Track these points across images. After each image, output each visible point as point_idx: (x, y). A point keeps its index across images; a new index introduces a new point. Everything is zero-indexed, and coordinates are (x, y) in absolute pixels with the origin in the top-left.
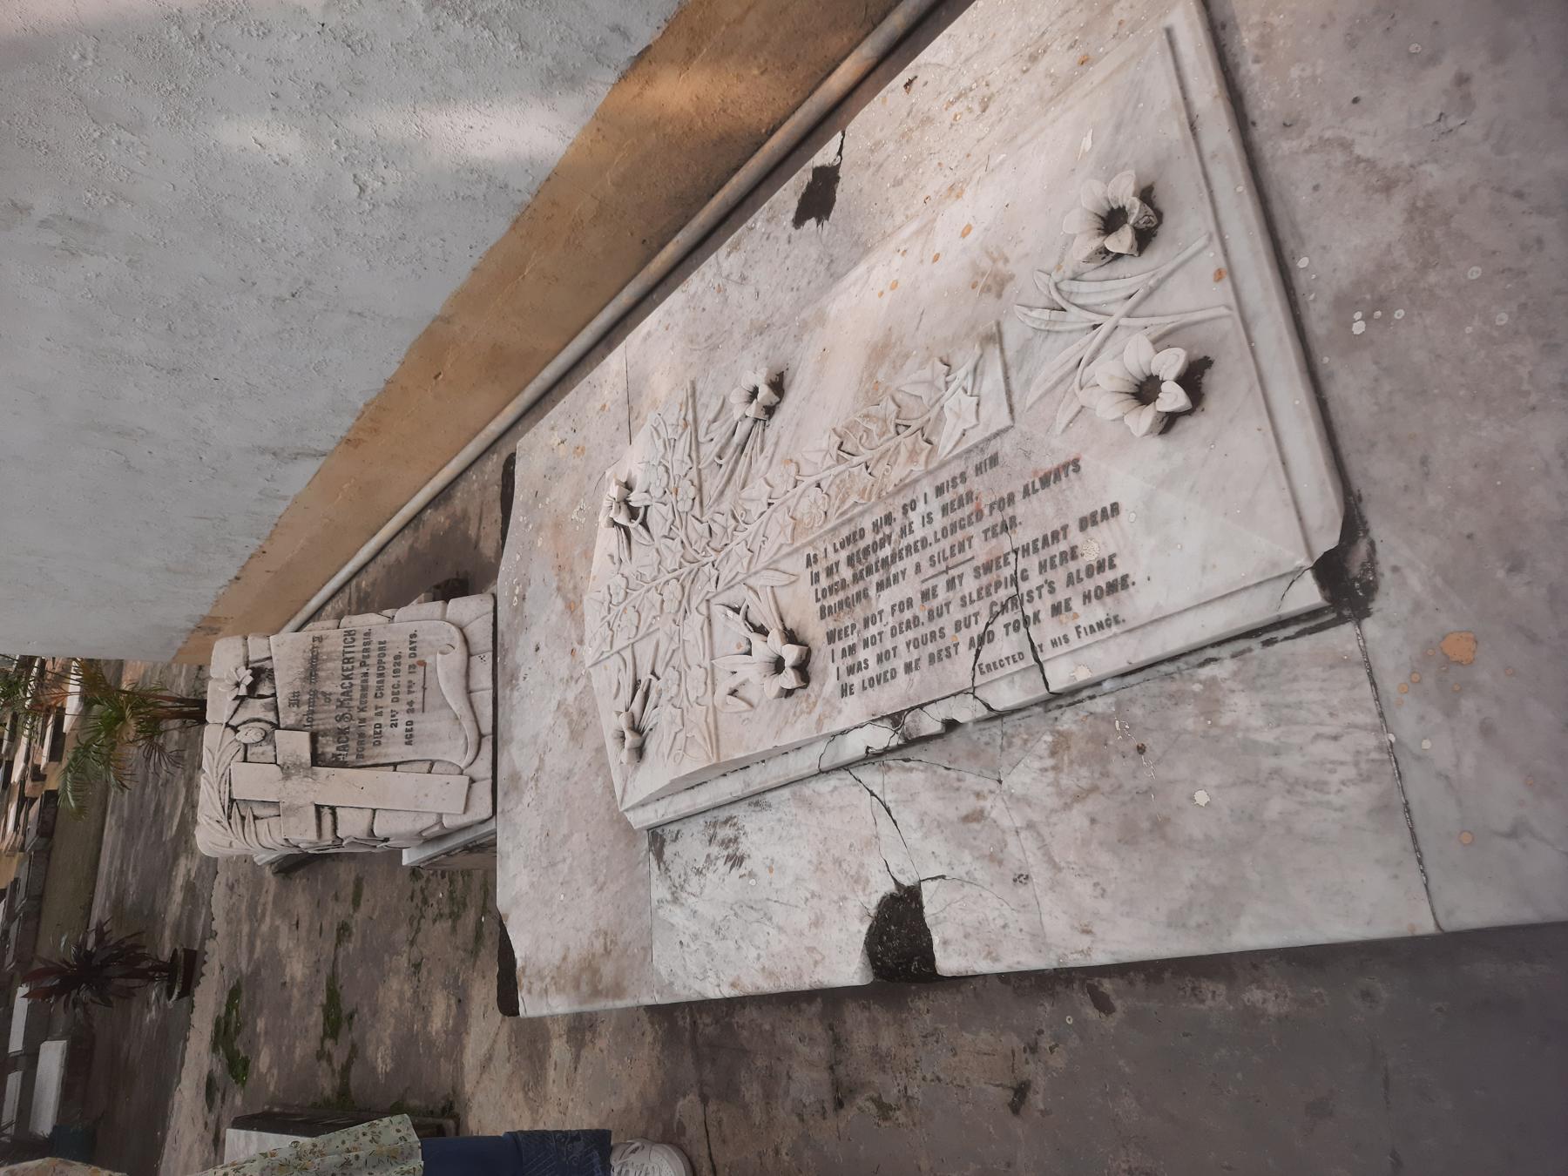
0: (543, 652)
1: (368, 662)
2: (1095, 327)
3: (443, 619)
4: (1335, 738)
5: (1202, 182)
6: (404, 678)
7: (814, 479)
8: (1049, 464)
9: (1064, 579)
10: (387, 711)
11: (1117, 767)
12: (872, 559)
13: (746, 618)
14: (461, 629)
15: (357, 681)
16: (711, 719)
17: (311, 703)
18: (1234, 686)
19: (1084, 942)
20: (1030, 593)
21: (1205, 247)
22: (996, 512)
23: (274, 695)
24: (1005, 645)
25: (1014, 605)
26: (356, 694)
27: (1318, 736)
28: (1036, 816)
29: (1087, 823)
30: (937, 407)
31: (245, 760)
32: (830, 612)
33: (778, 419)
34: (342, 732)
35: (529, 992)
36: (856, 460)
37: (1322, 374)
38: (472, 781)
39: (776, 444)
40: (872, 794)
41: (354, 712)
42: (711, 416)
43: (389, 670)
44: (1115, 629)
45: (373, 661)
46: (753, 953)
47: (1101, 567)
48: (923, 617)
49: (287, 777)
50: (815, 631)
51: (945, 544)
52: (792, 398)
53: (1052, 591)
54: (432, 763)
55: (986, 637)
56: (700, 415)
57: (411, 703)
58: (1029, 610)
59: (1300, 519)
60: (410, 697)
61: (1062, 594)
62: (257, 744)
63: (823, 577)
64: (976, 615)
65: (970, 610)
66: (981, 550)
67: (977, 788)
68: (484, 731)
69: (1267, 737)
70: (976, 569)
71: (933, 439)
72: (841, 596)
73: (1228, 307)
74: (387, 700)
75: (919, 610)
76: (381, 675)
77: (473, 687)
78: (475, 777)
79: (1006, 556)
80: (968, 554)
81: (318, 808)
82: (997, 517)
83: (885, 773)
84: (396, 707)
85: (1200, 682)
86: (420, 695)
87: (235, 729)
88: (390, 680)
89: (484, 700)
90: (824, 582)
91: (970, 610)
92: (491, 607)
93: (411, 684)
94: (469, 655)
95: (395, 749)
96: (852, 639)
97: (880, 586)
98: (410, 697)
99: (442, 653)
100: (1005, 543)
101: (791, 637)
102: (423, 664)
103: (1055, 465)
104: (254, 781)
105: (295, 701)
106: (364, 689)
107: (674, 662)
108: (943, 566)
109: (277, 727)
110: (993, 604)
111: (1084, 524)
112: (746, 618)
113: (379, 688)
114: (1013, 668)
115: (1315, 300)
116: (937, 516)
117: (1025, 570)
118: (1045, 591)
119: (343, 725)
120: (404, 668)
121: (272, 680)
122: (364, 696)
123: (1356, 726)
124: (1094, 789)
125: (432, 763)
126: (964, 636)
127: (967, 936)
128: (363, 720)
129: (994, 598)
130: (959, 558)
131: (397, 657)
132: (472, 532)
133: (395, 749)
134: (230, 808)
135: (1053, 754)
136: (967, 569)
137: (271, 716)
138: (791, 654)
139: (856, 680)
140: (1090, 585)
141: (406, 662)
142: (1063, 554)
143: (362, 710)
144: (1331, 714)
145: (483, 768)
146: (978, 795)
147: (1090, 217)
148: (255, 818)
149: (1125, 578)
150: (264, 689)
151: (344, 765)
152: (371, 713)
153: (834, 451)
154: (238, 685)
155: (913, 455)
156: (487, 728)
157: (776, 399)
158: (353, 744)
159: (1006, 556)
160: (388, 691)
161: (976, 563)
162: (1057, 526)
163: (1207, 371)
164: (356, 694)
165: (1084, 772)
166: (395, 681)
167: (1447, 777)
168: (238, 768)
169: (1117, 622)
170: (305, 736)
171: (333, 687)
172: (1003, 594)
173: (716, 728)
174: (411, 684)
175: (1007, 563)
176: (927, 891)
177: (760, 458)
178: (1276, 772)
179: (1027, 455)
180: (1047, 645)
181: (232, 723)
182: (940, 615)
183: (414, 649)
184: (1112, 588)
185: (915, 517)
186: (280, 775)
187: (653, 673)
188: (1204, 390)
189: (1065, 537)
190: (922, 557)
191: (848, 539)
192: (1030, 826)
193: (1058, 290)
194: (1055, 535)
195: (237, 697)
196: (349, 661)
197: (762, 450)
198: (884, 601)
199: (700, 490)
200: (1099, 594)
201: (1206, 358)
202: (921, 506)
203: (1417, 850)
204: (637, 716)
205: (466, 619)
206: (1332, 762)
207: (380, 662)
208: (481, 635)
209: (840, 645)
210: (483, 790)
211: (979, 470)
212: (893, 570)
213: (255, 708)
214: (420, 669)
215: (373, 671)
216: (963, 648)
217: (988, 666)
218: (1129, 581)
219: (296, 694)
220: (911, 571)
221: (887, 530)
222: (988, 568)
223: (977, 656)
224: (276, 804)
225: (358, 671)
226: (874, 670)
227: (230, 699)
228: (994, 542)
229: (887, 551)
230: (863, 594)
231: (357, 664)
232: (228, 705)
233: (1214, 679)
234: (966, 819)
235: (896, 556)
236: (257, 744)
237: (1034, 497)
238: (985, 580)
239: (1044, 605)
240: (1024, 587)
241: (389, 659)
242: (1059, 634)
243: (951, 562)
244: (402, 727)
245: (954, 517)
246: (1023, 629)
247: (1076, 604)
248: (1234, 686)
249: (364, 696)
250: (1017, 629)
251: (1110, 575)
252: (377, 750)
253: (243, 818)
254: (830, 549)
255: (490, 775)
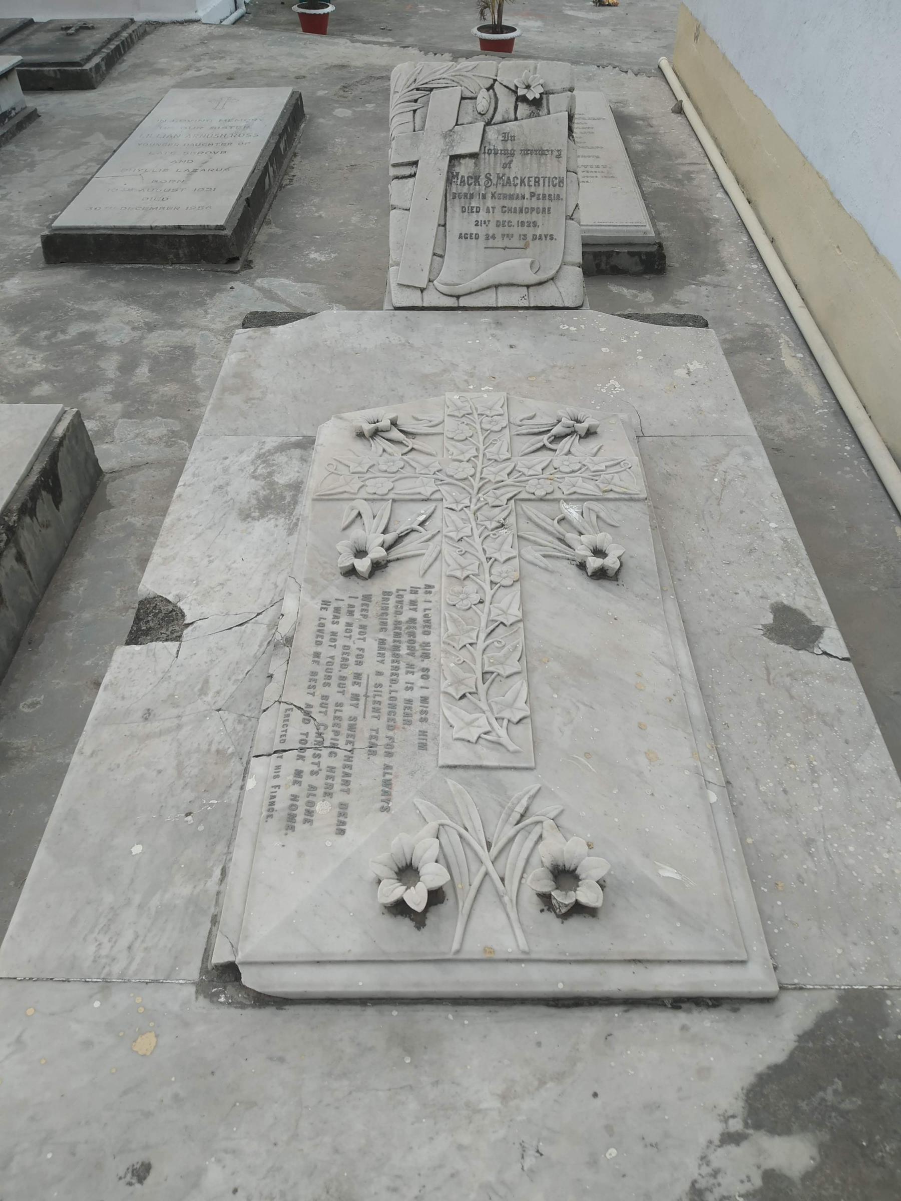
0: (508, 351)
1: (534, 199)
2: (489, 845)
3: (564, 263)
4: (130, 948)
5: (579, 958)
6: (516, 231)
7: (488, 599)
8: (396, 789)
9: (315, 784)
10: (490, 217)
11: (188, 795)
12: (405, 638)
13: (413, 531)
14: (552, 279)
15: (518, 190)
16: (345, 496)
17: (505, 152)
18: (198, 890)
19: (88, 751)
20: (319, 756)
21: (518, 946)
22: (387, 741)
23: (516, 119)
24: (297, 728)
25: (319, 743)
26: (508, 190)
27: (137, 937)
28: (184, 732)
29: (160, 767)
30: (485, 707)
31: (463, 98)
32: (384, 599)
33: (573, 571)
34: (476, 179)
35: (249, 338)
36: (482, 636)
37: (385, 1008)
38: (422, 290)
39: (546, 569)
40: (259, 614)
41: (492, 189)
42: (602, 515)
43: (524, 217)
44: (265, 813)
45: (535, 203)
46: (193, 512)
47: (309, 813)
48: (345, 672)
49: (445, 136)
50: (375, 588)
51: (385, 699)
52: (591, 587)
53: (313, 773)
54: (442, 256)
55: (308, 716)
56: (611, 505)
57: (494, 237)
58: (309, 753)
59: (273, 963)
60: (499, 237)
61: (307, 779)
62: (475, 108)
63: (413, 597)
64: (326, 713)
65: (331, 709)
66: (365, 726)
67: (222, 694)
68: (461, 299)
69: (155, 902)
70: (355, 719)
71: (464, 701)
72: (391, 610)
73: (458, 952)
74: (499, 216)
75: (352, 669)
76: (521, 211)
77: (500, 289)
78: (425, 293)
79: (352, 743)
80: (369, 714)
81: (415, 163)
82: (382, 741)
83: (268, 626)
84: (492, 225)
85: (212, 867)
86: (500, 244)
87: (491, 87)
88: (515, 218)
89: (488, 299)
90: (408, 597)
91: (331, 709)
92: (567, 305)
93: (510, 236)
94: (528, 286)
95: (458, 223)
96: (357, 615)
97: (382, 642)
98: (499, 237)
99: (532, 263)
100: (361, 743)
101: (378, 567)
102: (526, 247)
103: (394, 793)
104: (443, 104)
105: (507, 137)
106: (511, 197)
107: (408, 468)
108: (371, 694)
109: (488, 123)
110: (326, 727)
111: (343, 806)
112: (413, 531)
113: (510, 210)
114: (279, 732)
115: (447, 1018)
116: (408, 695)
117: (336, 754)
118: (315, 768)
119: (482, 180)
120: (525, 230)
121: (530, 116)
122: (505, 197)
123: (130, 963)
124: (180, 774)
125: (442, 256)
126: (316, 701)
127: (130, 670)
128: (484, 197)
129: (330, 728)
130: (370, 706)
131: (535, 224)
132: (707, 278)
133: (458, 223)
134: (425, 90)
135: (218, 752)
136: (358, 712)
137: (498, 118)
138: (363, 565)
139: (329, 614)
140: (301, 804)
141: (530, 232)
142: (332, 786)
143: (493, 196)
144: (146, 949)
145: (432, 298)
146: (218, 692)
147: (575, 862)
148: (415, 111)
149: (292, 828)
150: (523, 109)
151: (449, 181)
152: (490, 203)
153: (501, 619)
154: (528, 87)
155: (459, 682)
156: (463, 302)
157: (590, 571)
158: (465, 189)
159: (352, 743)
160: (506, 217)
161: (360, 718)
162: (353, 786)
163: (413, 924)
164: (508, 190)
165: (195, 771)
166: (514, 223)
167: (71, 1011)
168: (456, 93)
169: (268, 816)
170: (476, 149)
171: (515, 170)
172: (329, 736)
173: (338, 500)
174: (510, 236)
175: (348, 742)
176: (172, 646)
177: (538, 554)
178: (128, 902)
179: (412, 774)
180: (280, 762)
181: (497, 85)
182: (339, 685)
183: (540, 238)
184: (291, 818)
185: (416, 678)
186: (446, 129)
187: (413, 449)
188: (399, 918)
189: (342, 790)
190: (385, 680)
191: (428, 621)
192: (179, 727)
193: (537, 823)
194: (347, 783)
195: (517, 87)
196: (537, 182)
197: (544, 556)
198: (371, 645)
199: (541, 500)
200: (293, 807)
201: (424, 925)
202: (421, 683)
203: (38, 980)
204: (386, 435)
205: (559, 284)
206: (115, 942)
207: (533, 209)
208: (547, 296)
209: (358, 603)
210: (414, 299)
211: (423, 733)
212: (388, 654)
213: (506, 103)
214: (522, 244)
215: (526, 203)
216: (309, 699)
217: (288, 715)
218: (289, 832)
219: (513, 138)
220: (381, 667)
221: (418, 654)
222: (352, 728)
223: (299, 708)
224: (423, 128)
225: (526, 191)
226: (330, 627)
227: (516, 82)
228: (367, 735)
229: (404, 651)
230: (383, 627)
231: (533, 189)
232: (514, 80)
233: (210, 876)
234: (206, 682)
235: (396, 657)
236: (475, 108)
237: (381, 772)
238: (345, 724)
239: (307, 767)
240: (325, 752)
241: (534, 217)
242: (282, 772)
243: (370, 699)
244: (474, 230)
245: (400, 705)
246: (298, 746)
247: (295, 789)
248: (198, 890)
249: (505, 197)
250: (301, 741)
251: (300, 818)
252: (458, 209)
253: (416, 101)
254: (428, 605)
255: (425, 305)
